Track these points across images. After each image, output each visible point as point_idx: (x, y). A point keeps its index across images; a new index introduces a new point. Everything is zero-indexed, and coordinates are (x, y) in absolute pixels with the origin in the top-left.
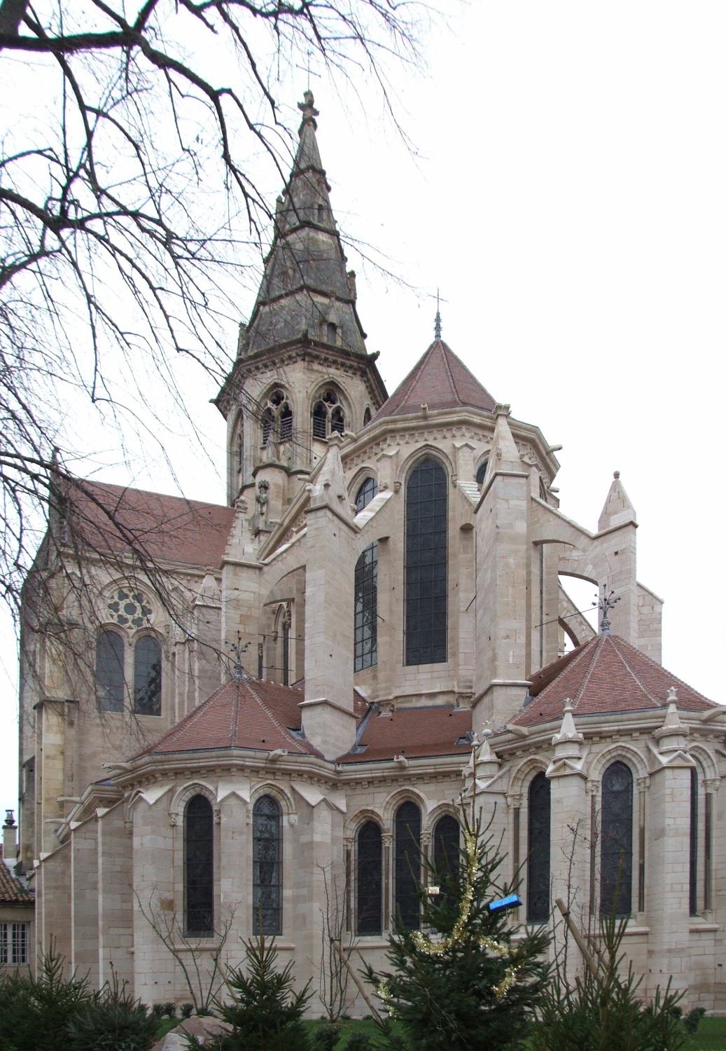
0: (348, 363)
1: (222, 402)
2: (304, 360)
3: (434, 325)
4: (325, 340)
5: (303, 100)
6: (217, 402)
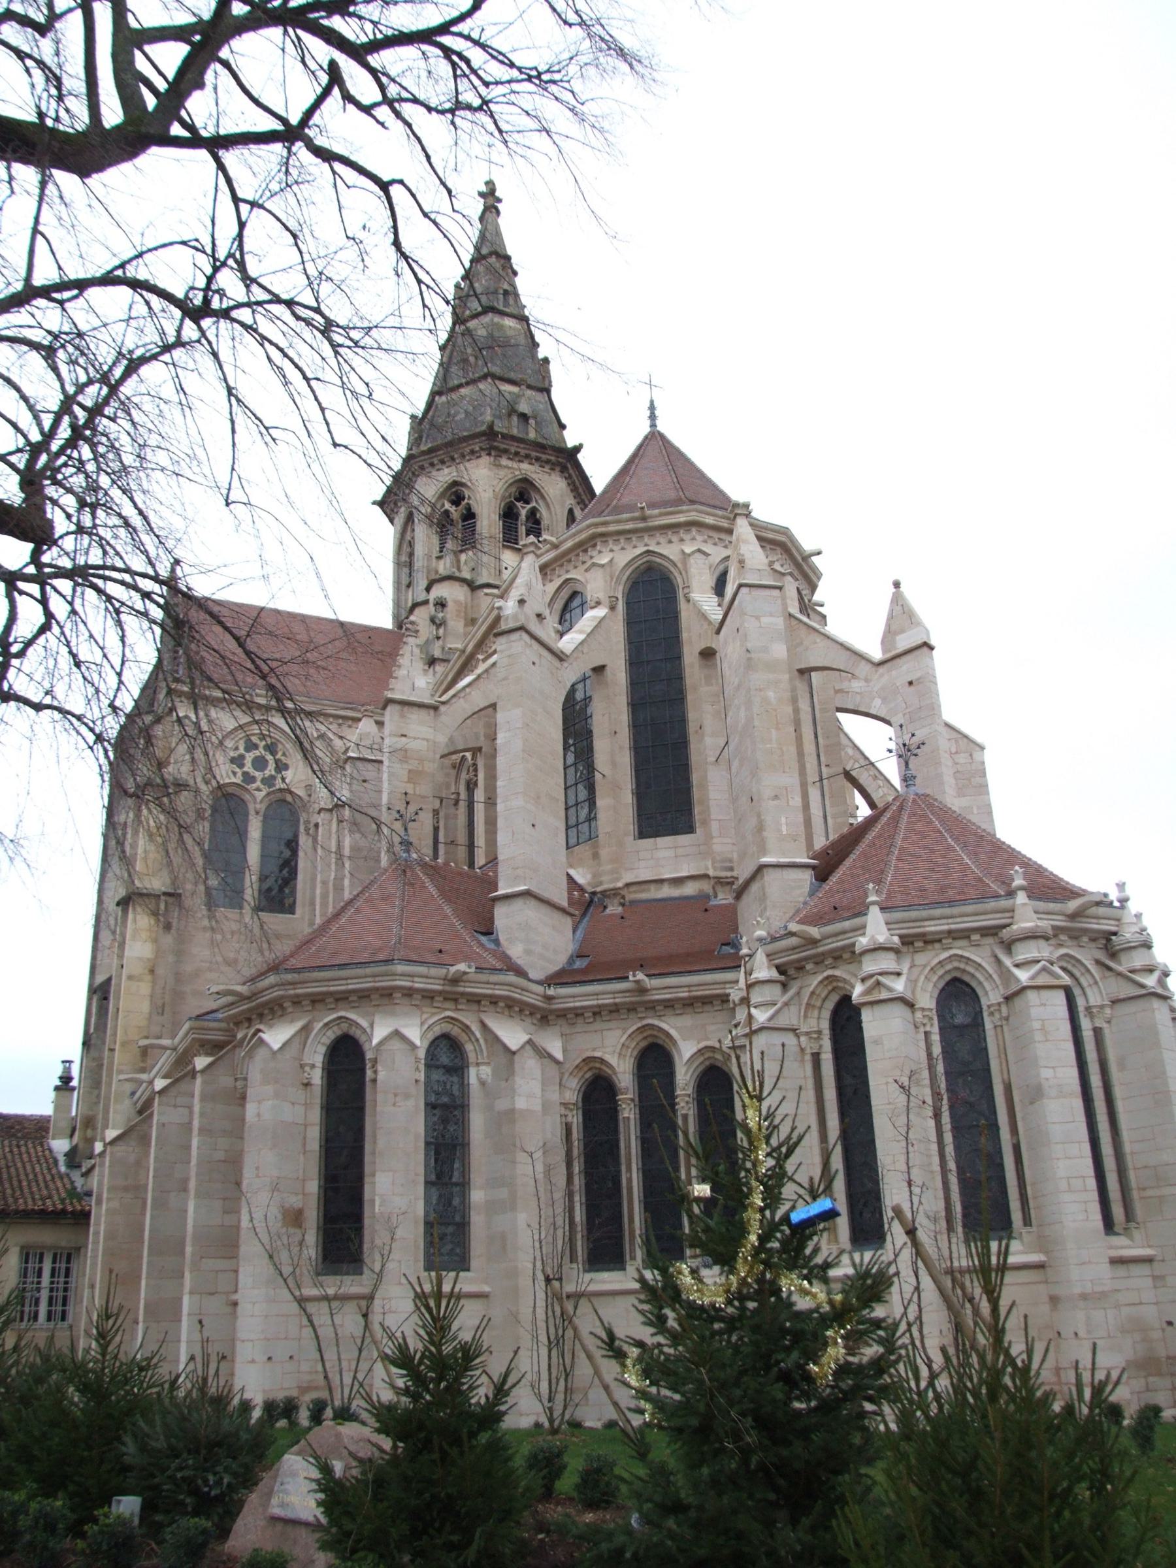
0: (544, 457)
2: (489, 454)
3: (648, 413)
4: (515, 432)
6: (381, 504)
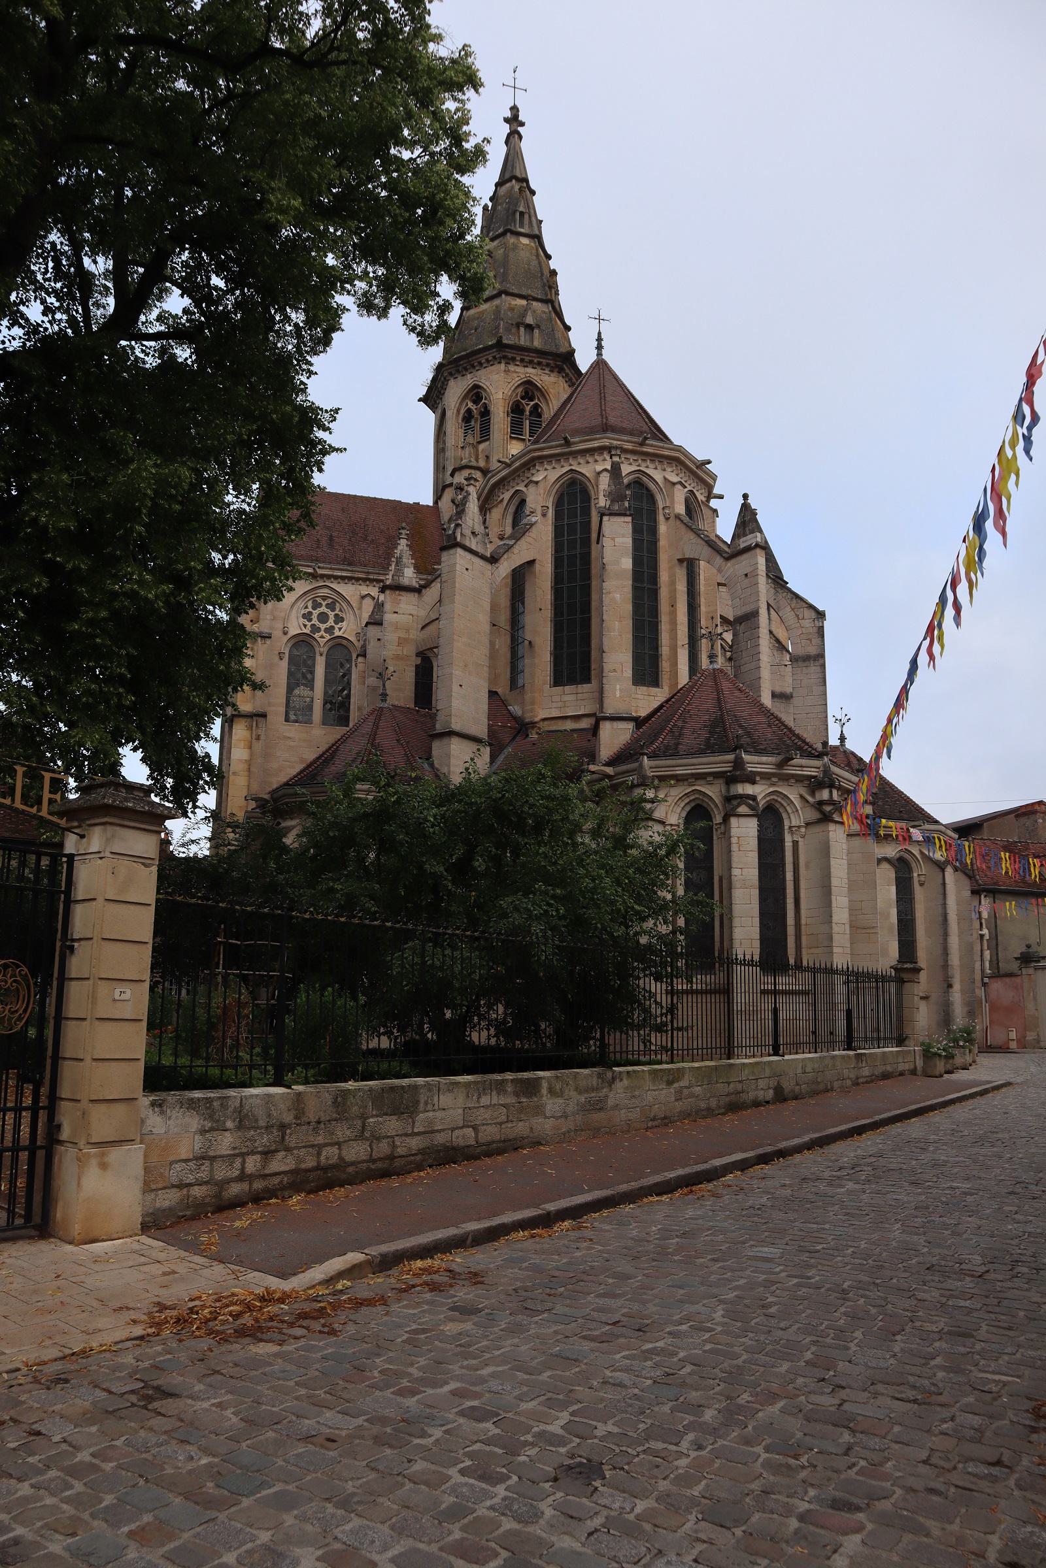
1: (432, 398)
5: (508, 114)
6: (425, 399)
